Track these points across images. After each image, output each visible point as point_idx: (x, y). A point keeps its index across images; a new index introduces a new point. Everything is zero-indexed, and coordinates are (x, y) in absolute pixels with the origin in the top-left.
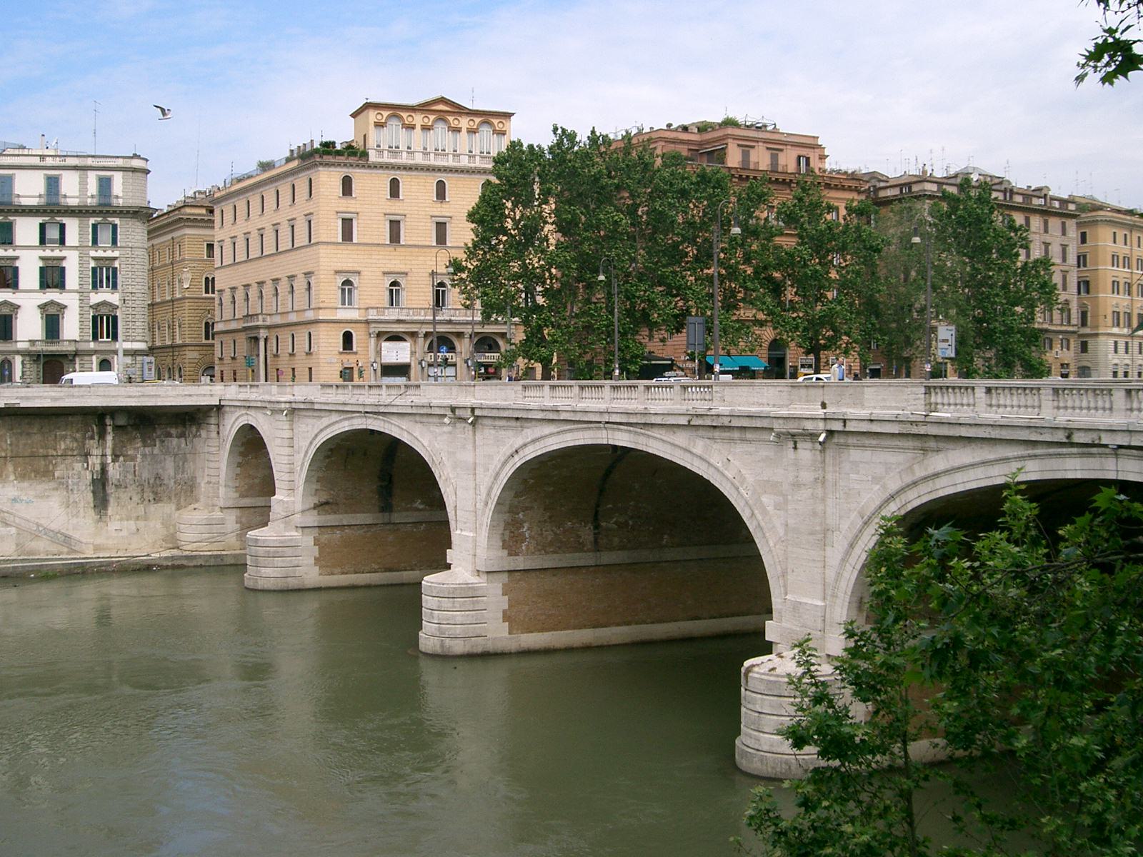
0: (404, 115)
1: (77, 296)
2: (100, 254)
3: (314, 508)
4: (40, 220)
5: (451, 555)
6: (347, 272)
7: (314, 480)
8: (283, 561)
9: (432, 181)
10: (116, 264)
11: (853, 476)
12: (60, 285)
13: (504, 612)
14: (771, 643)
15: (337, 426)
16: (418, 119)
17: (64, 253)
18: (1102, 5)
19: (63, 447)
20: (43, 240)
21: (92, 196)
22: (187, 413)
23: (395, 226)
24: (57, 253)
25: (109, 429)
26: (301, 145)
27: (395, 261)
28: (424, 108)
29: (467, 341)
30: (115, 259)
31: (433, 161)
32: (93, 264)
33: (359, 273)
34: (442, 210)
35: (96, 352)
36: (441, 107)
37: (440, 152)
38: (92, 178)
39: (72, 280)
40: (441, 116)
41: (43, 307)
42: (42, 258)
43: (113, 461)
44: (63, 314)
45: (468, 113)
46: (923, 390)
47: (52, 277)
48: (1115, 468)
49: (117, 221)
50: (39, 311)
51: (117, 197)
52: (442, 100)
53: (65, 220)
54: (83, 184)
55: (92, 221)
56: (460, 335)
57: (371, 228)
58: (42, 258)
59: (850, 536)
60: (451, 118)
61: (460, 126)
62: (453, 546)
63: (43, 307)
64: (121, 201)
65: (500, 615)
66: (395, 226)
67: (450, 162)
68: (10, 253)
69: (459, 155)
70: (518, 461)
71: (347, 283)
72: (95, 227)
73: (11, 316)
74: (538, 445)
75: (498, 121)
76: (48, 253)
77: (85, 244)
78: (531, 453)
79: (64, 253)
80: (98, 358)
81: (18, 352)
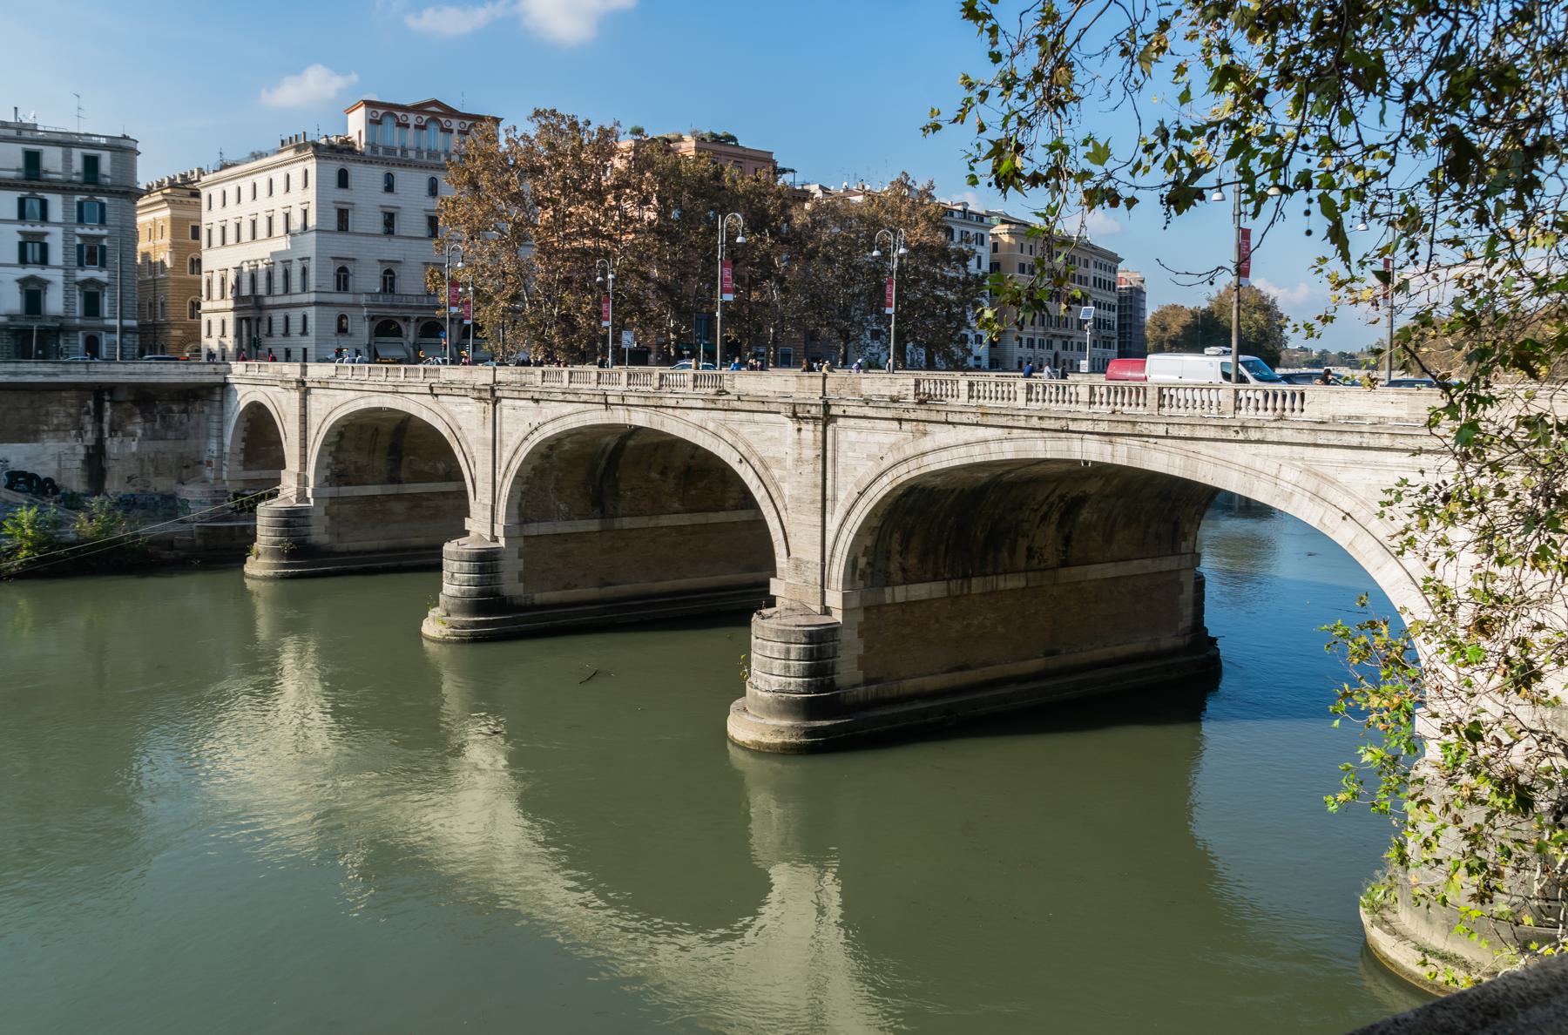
0: (399, 114)
1: (61, 272)
2: (87, 231)
4: (18, 194)
5: (469, 524)
7: (327, 454)
8: (514, 622)
10: (105, 242)
11: (851, 454)
12: (44, 261)
13: (520, 573)
14: (774, 597)
15: (352, 404)
16: (412, 119)
17: (46, 229)
20: (22, 216)
21: (77, 174)
24: (38, 228)
25: (107, 405)
26: (300, 133)
27: (391, 249)
28: (418, 109)
29: (413, 325)
30: (104, 237)
32: (78, 241)
33: (353, 259)
35: (82, 328)
36: (434, 109)
38: (77, 155)
39: (56, 255)
40: (434, 118)
41: (23, 282)
42: (20, 232)
43: (111, 436)
48: (1274, 472)
49: (105, 200)
51: (105, 176)
52: (436, 103)
53: (47, 196)
54: (67, 159)
55: (78, 198)
56: (406, 319)
58: (20, 232)
59: (848, 506)
60: (443, 120)
63: (23, 282)
64: (108, 180)
65: (517, 575)
70: (537, 438)
71: (343, 270)
72: (80, 204)
74: (557, 423)
76: (28, 228)
78: (549, 431)
79: (46, 229)
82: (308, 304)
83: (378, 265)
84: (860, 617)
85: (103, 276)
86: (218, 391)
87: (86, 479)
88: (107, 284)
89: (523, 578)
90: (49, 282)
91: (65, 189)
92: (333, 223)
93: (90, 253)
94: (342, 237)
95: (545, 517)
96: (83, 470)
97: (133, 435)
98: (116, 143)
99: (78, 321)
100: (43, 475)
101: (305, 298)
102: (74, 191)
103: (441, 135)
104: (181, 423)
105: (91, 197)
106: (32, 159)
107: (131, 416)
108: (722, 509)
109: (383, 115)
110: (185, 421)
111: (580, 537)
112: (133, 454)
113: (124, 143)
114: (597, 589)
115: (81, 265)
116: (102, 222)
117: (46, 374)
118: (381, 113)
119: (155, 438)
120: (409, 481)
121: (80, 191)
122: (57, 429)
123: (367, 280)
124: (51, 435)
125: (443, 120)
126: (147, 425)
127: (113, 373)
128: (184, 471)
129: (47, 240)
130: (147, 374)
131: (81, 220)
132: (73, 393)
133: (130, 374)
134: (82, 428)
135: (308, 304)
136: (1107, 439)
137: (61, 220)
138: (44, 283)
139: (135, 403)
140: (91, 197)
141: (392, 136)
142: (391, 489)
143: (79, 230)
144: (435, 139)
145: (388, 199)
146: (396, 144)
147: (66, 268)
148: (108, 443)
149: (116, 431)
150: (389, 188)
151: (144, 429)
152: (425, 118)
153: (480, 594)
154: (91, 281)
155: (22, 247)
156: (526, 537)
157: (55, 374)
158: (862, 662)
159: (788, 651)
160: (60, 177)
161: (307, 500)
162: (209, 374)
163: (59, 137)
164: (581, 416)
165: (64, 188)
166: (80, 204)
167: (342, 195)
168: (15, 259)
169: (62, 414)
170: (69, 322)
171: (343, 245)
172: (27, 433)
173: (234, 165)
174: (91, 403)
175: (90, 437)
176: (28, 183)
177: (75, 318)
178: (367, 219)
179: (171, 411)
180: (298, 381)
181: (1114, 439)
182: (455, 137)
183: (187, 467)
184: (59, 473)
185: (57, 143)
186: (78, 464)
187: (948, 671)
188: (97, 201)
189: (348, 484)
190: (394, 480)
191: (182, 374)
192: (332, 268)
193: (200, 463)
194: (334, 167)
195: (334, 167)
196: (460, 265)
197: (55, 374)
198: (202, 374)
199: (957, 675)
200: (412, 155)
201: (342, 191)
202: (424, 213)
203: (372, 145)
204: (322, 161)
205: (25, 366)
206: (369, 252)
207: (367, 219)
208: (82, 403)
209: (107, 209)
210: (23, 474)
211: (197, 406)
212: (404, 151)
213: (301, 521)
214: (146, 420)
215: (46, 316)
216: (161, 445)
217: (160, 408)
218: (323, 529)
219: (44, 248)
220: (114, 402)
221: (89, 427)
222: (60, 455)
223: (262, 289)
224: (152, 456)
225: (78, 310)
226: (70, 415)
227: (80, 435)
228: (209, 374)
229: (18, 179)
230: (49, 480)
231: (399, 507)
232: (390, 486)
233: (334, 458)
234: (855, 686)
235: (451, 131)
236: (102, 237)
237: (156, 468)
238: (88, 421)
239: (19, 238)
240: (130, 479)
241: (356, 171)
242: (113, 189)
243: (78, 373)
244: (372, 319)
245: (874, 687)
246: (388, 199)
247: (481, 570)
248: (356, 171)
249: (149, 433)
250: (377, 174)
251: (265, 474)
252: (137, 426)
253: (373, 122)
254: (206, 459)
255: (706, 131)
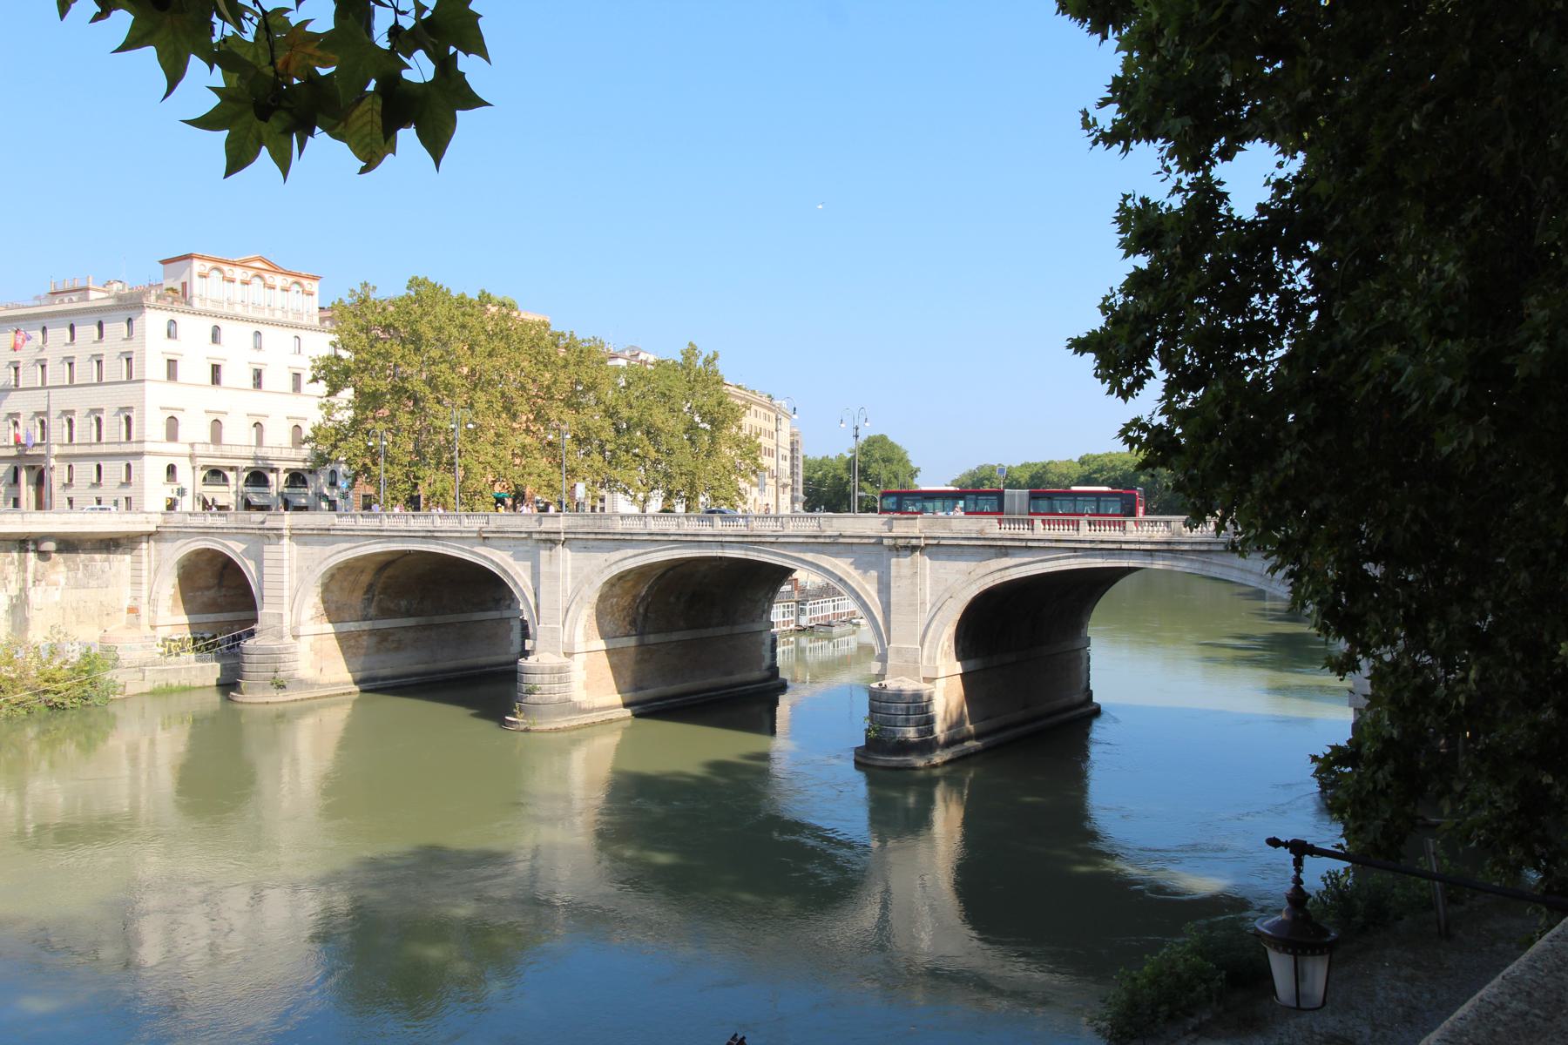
0: (226, 268)
3: (312, 619)
6: (297, 418)
9: (209, 323)
18: (1152, 378)
27: (217, 398)
31: (252, 314)
37: (257, 307)
43: (34, 585)
45: (282, 273)
46: (996, 521)
57: (237, 375)
60: (267, 276)
61: (312, 290)
67: (266, 315)
69: (274, 310)
75: (229, 268)
89: (586, 686)
97: (56, 584)
119: (78, 586)
130: (81, 523)
133: (66, 523)
134: (6, 578)
136: (1149, 553)
150: (215, 337)
162: (142, 523)
164: (188, 546)
175: (14, 589)
179: (94, 560)
181: (1153, 553)
196: (1469, 522)
214: (69, 570)
216: (82, 593)
221: (13, 577)
228: (142, 523)
237: (78, 616)
249: (72, 582)
251: (243, 615)
255: (487, 292)
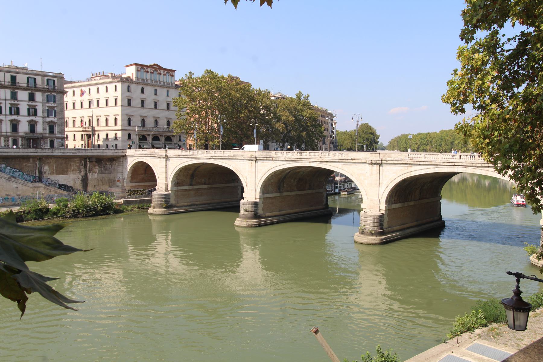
0: (145, 68)
1: (42, 119)
2: (50, 105)
10: (56, 109)
12: (36, 114)
19: (73, 168)
22: (112, 158)
23: (143, 102)
28: (151, 66)
29: (151, 137)
30: (55, 107)
32: (47, 108)
33: (133, 115)
34: (169, 99)
35: (49, 137)
36: (156, 67)
39: (40, 113)
40: (156, 70)
41: (11, 121)
42: (28, 105)
43: (89, 172)
44: (19, 123)
47: (32, 111)
49: (55, 94)
50: (27, 123)
52: (156, 65)
54: (43, 80)
55: (46, 94)
57: (150, 104)
58: (28, 105)
60: (158, 70)
62: (245, 192)
63: (11, 121)
66: (143, 102)
68: (16, 102)
70: (273, 170)
72: (47, 96)
73: (35, 125)
77: (44, 101)
80: (12, 138)
81: (20, 136)
82: (118, 130)
83: (140, 117)
84: (387, 212)
85: (55, 120)
86: (122, 158)
87: (82, 186)
88: (57, 123)
90: (20, 121)
91: (43, 90)
92: (126, 104)
93: (49, 112)
94: (129, 108)
95: (268, 193)
96: (81, 183)
97: (96, 172)
98: (59, 75)
99: (47, 135)
100: (69, 185)
101: (116, 128)
102: (45, 91)
103: (145, 73)
104: (110, 168)
105: (51, 93)
106: (13, 79)
107: (95, 166)
108: (305, 190)
109: (141, 68)
110: (111, 168)
111: (275, 198)
112: (96, 178)
113: (61, 76)
114: (279, 212)
115: (48, 116)
116: (55, 102)
117: (73, 153)
118: (140, 67)
119: (102, 173)
120: (195, 185)
121: (48, 91)
122: (73, 170)
123: (136, 122)
124: (72, 172)
125: (158, 70)
126: (100, 169)
127: (93, 153)
128: (111, 184)
129: (37, 107)
131: (48, 101)
132: (78, 159)
133: (98, 153)
134: (81, 170)
135: (118, 130)
137: (41, 101)
138: (36, 122)
139: (96, 162)
140: (51, 93)
141: (144, 75)
142: (191, 187)
143: (47, 105)
144: (156, 76)
145: (142, 96)
146: (145, 78)
147: (43, 118)
148: (88, 175)
149: (91, 171)
151: (99, 170)
152: (153, 69)
153: (255, 214)
154: (51, 122)
155: (29, 109)
156: (264, 198)
157: (75, 153)
158: (388, 222)
159: (374, 220)
160: (41, 86)
161: (168, 191)
162: (121, 153)
163: (40, 73)
165: (42, 90)
166: (47, 96)
167: (129, 94)
168: (26, 114)
169: (75, 165)
170: (44, 135)
171: (129, 110)
172: (64, 172)
173: (75, 82)
174: (83, 162)
175: (83, 173)
176: (12, 86)
177: (46, 134)
178: (136, 102)
179: (106, 164)
180: (166, 155)
182: (149, 74)
183: (111, 182)
184: (74, 185)
185: (40, 75)
186: (80, 181)
187: (401, 225)
188: (53, 95)
189: (180, 186)
190: (191, 185)
191: (113, 153)
192: (126, 118)
193: (115, 181)
194: (126, 85)
195: (126, 85)
197: (75, 153)
198: (119, 153)
199: (403, 226)
200: (149, 81)
201: (142, 95)
202: (166, 102)
203: (137, 78)
204: (123, 83)
205: (29, 150)
206: (137, 113)
207: (136, 102)
208: (81, 162)
209: (56, 97)
210: (63, 185)
211: (114, 163)
212: (147, 80)
213: (168, 197)
214: (99, 168)
215: (37, 133)
216: (104, 175)
217: (103, 163)
218: (173, 200)
219: (36, 110)
220: (90, 162)
222: (74, 179)
223: (95, 124)
224: (101, 179)
225: (47, 131)
226: (77, 166)
227: (80, 172)
228: (121, 153)
229: (8, 85)
230: (71, 187)
231: (192, 193)
232: (190, 186)
233: (177, 178)
234: (386, 228)
235: (161, 74)
236: (54, 107)
237: (103, 183)
238: (82, 167)
239: (28, 107)
240: (95, 186)
241: (133, 87)
242: (59, 91)
243: (82, 152)
244: (139, 135)
245: (390, 229)
246: (142, 96)
247: (255, 207)
248: (133, 87)
249: (100, 171)
250: (139, 88)
252: (97, 169)
253: (138, 71)
254: (117, 179)
